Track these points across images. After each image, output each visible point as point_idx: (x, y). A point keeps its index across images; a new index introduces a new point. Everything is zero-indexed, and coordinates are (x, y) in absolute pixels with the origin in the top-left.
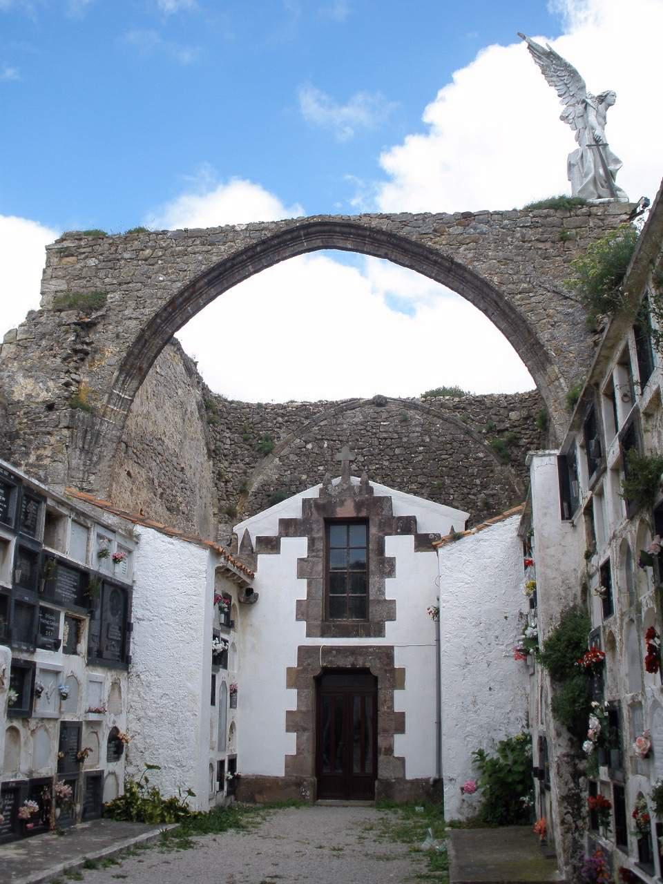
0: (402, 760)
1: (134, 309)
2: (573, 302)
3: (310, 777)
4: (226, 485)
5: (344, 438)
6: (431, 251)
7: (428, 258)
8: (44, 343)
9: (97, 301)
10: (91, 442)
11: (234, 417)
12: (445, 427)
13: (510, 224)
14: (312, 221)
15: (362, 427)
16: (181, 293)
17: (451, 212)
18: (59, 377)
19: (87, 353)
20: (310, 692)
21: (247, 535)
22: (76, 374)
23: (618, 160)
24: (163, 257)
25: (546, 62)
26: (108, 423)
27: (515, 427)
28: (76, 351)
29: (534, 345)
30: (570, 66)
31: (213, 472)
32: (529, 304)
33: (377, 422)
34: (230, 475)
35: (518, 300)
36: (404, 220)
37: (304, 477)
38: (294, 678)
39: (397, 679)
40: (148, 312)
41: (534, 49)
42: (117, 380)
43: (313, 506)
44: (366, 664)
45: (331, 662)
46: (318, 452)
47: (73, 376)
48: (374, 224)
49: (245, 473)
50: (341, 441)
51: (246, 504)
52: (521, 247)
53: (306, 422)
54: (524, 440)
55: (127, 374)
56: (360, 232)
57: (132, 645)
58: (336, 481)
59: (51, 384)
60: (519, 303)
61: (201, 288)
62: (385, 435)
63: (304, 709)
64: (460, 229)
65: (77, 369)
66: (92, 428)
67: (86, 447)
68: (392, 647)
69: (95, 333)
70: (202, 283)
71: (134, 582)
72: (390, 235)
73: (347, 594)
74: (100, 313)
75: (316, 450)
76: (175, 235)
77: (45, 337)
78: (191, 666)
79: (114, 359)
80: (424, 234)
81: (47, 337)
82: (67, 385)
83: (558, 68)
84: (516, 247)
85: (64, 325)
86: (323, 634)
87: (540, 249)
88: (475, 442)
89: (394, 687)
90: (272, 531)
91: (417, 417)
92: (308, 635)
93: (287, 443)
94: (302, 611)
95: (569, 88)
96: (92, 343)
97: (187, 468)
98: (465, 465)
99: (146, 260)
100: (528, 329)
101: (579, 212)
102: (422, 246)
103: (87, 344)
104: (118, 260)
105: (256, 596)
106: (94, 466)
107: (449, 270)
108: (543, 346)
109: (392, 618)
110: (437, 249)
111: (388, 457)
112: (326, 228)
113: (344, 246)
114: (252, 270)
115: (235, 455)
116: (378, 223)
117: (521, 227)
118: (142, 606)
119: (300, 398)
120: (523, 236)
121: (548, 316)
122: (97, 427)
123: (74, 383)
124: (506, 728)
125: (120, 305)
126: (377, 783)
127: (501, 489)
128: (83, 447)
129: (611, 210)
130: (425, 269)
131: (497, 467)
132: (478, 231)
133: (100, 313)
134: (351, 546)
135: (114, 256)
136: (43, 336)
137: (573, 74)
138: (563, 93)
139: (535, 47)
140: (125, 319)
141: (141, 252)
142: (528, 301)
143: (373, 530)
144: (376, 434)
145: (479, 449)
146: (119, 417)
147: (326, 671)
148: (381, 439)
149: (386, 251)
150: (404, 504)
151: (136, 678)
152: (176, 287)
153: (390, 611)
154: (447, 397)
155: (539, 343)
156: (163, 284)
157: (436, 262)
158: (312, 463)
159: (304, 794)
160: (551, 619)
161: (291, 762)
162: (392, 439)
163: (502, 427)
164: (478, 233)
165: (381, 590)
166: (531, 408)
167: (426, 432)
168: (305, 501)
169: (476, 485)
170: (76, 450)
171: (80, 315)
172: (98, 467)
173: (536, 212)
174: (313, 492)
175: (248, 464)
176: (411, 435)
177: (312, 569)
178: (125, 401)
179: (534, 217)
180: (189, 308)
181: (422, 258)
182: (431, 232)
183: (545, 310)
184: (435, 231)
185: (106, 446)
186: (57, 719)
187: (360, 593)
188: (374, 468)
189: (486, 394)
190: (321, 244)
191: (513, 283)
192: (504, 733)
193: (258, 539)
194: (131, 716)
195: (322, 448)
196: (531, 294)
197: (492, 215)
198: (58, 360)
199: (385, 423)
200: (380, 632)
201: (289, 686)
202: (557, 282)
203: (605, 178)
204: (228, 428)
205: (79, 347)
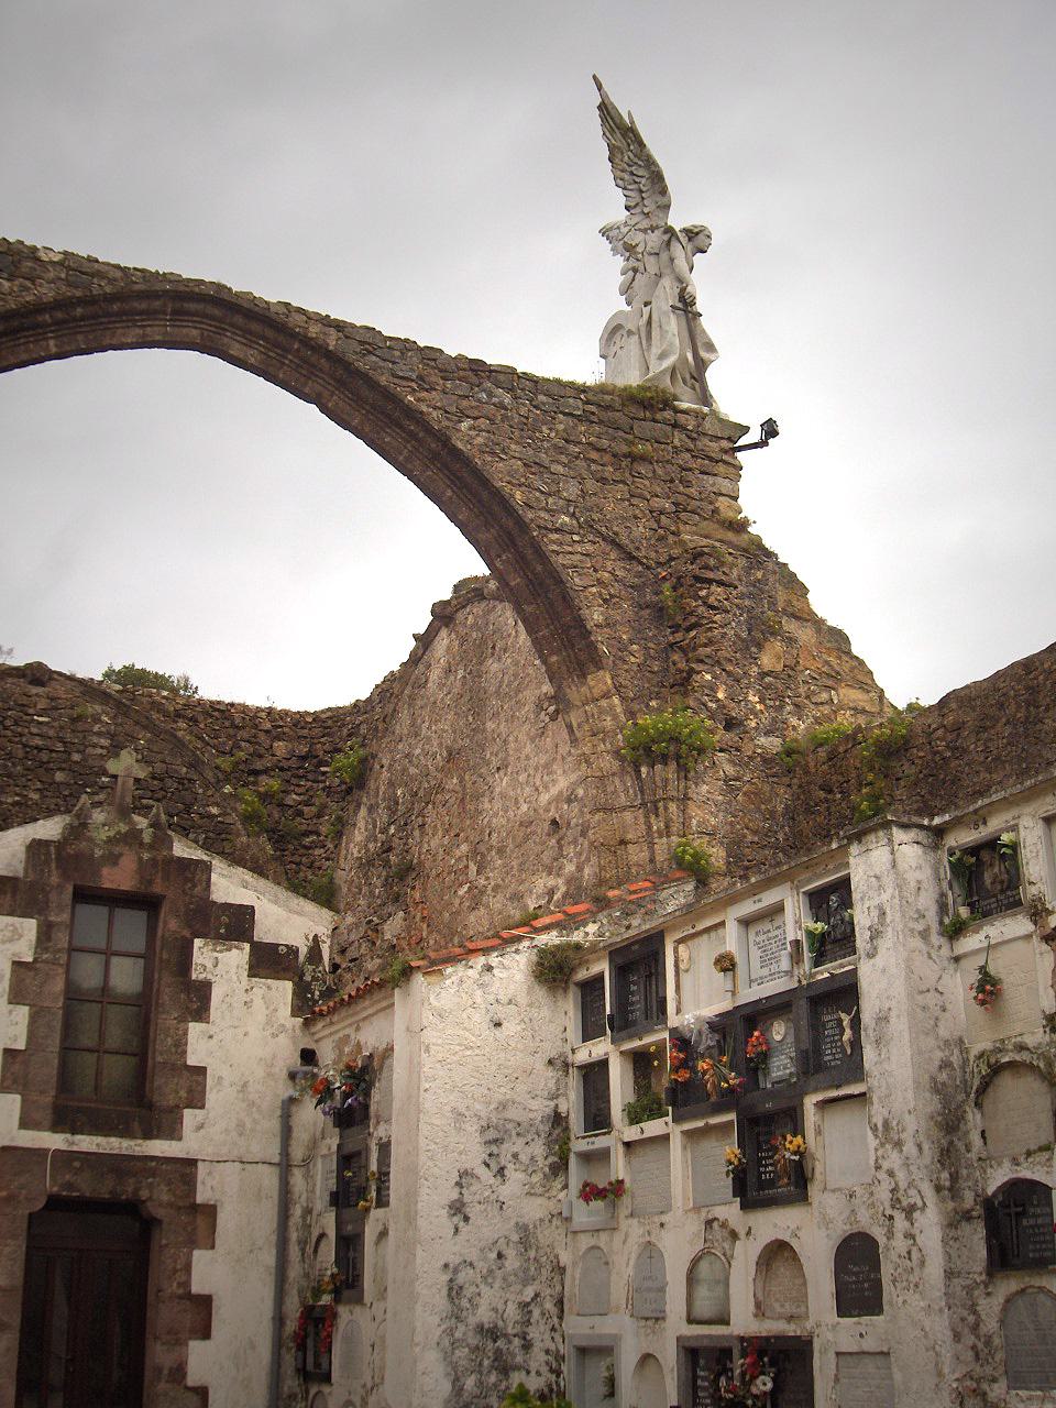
2: (640, 568)
13: (548, 403)
14: (197, 290)
17: (451, 351)
23: (713, 345)
25: (619, 142)
30: (654, 163)
32: (571, 553)
33: (27, 714)
41: (609, 113)
44: (141, 1193)
48: (314, 330)
54: (294, 796)
56: (281, 338)
62: (38, 741)
83: (636, 160)
84: (555, 446)
88: (206, 786)
89: (192, 1243)
92: (25, 1124)
95: (643, 198)
101: (658, 416)
102: (396, 400)
110: (422, 412)
111: (39, 785)
114: (54, 350)
121: (600, 582)
132: (495, 400)
137: (657, 178)
138: (633, 204)
139: (612, 112)
142: (570, 549)
143: (171, 924)
144: (21, 735)
145: (212, 799)
147: (54, 1203)
148: (30, 747)
157: (413, 435)
162: (52, 751)
163: (258, 765)
165: (181, 1045)
166: (316, 741)
174: (49, 829)
176: (90, 750)
183: (596, 571)
184: (421, 378)
188: (10, 800)
191: (548, 511)
196: (576, 538)
199: (41, 719)
200: (174, 1132)
203: (693, 370)
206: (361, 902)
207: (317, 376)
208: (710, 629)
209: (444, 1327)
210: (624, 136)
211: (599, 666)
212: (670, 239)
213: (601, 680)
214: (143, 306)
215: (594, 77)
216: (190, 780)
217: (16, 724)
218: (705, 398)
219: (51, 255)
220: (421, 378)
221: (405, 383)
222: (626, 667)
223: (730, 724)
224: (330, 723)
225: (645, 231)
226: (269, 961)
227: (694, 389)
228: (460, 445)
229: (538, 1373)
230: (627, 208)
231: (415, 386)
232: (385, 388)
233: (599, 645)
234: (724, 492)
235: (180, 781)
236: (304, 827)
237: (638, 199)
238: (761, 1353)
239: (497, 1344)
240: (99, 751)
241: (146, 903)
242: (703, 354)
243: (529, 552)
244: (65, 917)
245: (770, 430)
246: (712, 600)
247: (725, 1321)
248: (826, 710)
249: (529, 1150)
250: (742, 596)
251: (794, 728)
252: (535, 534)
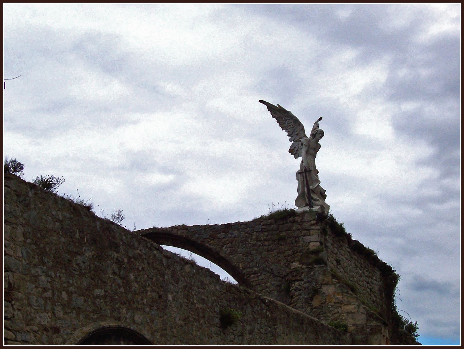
121: (267, 287)
184: (210, 236)
196: (259, 274)
197: (241, 225)
215: (260, 101)
221: (206, 240)
228: (223, 255)
231: (208, 240)
248: (336, 316)
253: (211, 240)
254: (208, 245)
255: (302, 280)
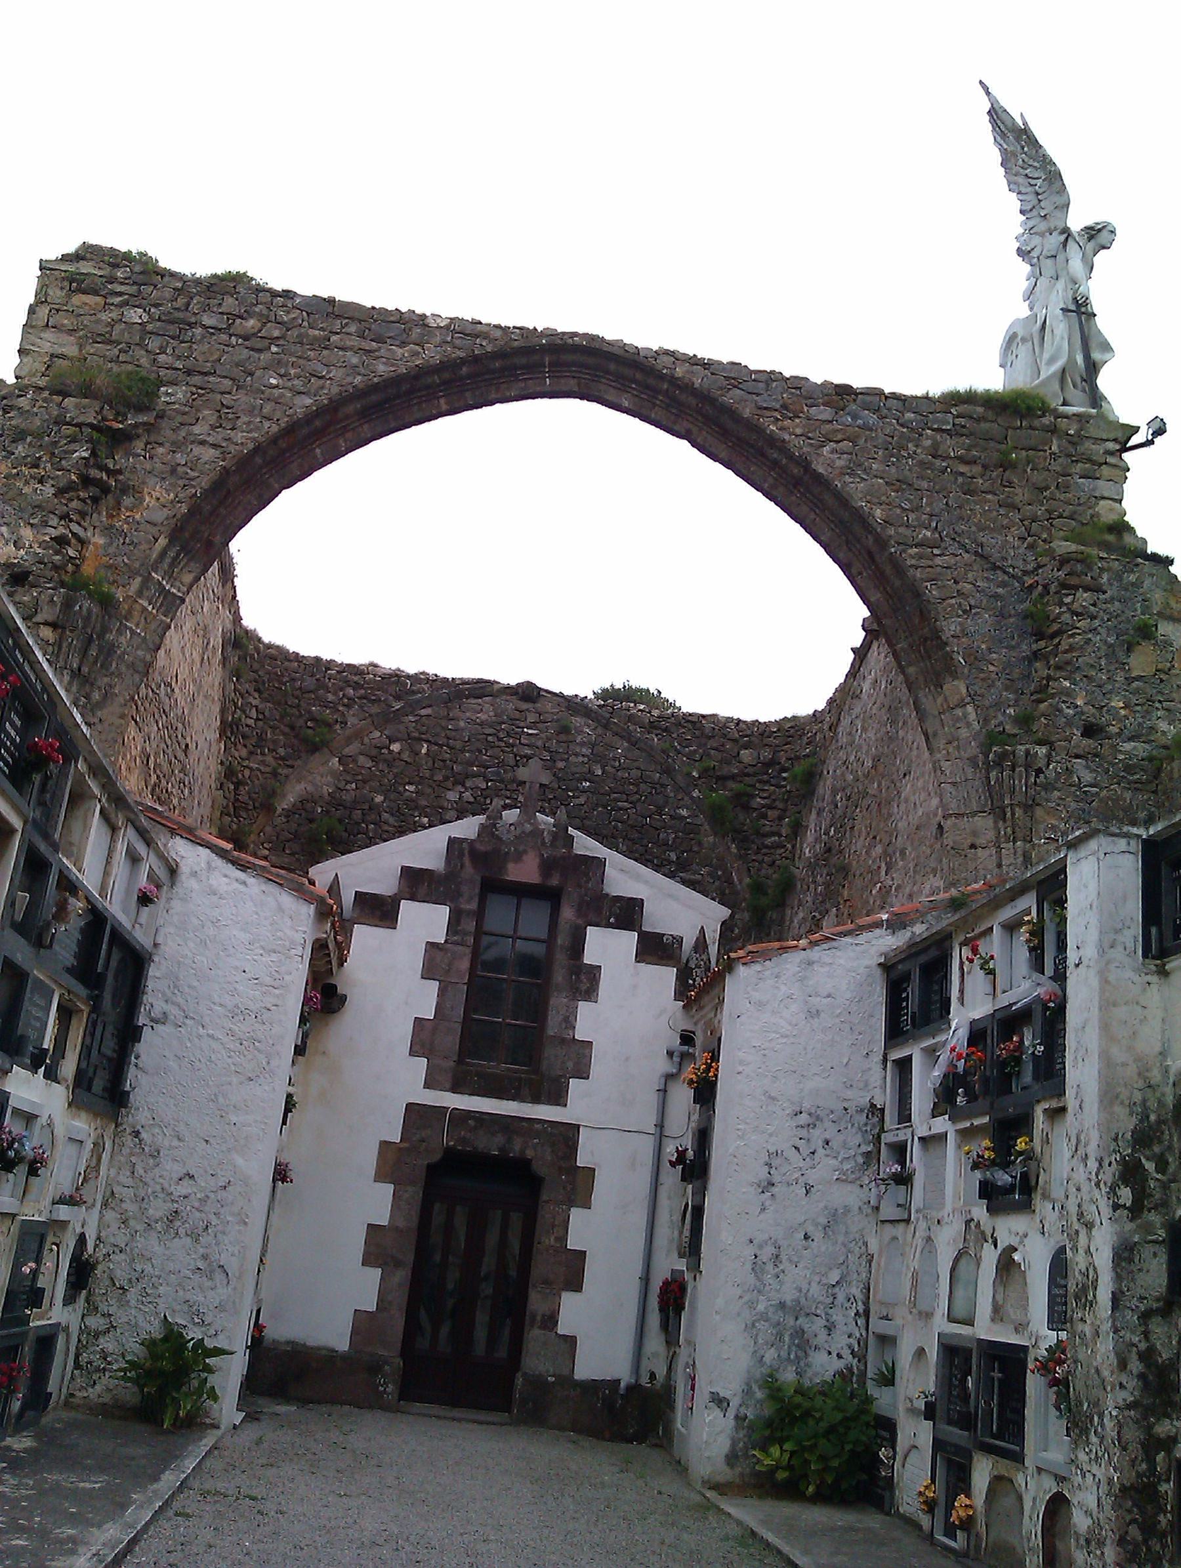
0: (571, 1341)
1: (213, 427)
3: (390, 1352)
4: (236, 789)
5: (458, 745)
6: (772, 441)
7: (763, 455)
8: (20, 450)
9: (139, 396)
10: (95, 662)
11: (269, 673)
12: (629, 755)
15: (491, 731)
16: (310, 418)
17: (817, 379)
18: (46, 522)
19: (106, 490)
20: (414, 1193)
21: (334, 888)
22: (79, 524)
24: (281, 342)
25: (1014, 147)
26: (133, 632)
27: (748, 775)
28: (86, 481)
29: (926, 639)
31: (222, 763)
34: (247, 773)
35: (912, 557)
36: (732, 375)
37: (379, 799)
38: (391, 1163)
39: (579, 1186)
40: (243, 438)
42: (163, 554)
43: (466, 852)
45: (463, 1141)
46: (409, 760)
47: (75, 528)
48: (679, 371)
49: (275, 774)
50: (451, 748)
51: (268, 829)
52: (930, 466)
53: (397, 705)
55: (183, 548)
57: (132, 1069)
58: (511, 815)
59: (27, 533)
60: (913, 562)
61: (347, 417)
63: (401, 1223)
64: (826, 413)
65: (83, 514)
66: (101, 636)
67: (85, 670)
68: (578, 1126)
69: (128, 454)
70: (350, 409)
71: (156, 945)
72: (704, 397)
73: (505, 1018)
74: (143, 418)
75: (406, 756)
76: (308, 305)
77: (24, 439)
78: (250, 1125)
79: (160, 513)
80: (766, 408)
81: (29, 439)
82: (61, 541)
84: (922, 463)
85: (68, 424)
86: (456, 1087)
87: (962, 474)
88: (678, 788)
89: (571, 1203)
90: (385, 885)
91: (586, 730)
92: (427, 1085)
93: (358, 735)
94: (423, 1039)
95: (1040, 201)
96: (120, 472)
97: (192, 746)
98: (658, 824)
99: (246, 338)
100: (921, 611)
101: (1036, 423)
102: (759, 430)
103: (110, 472)
104: (190, 324)
105: (344, 998)
106: (92, 710)
107: (797, 482)
108: (946, 644)
109: (583, 1073)
112: (591, 361)
113: (615, 400)
114: (444, 407)
115: (260, 738)
116: (687, 372)
117: (933, 430)
118: (164, 994)
119: (389, 661)
120: (936, 445)
121: (960, 593)
122: (110, 637)
123: (73, 541)
124: (827, 1314)
125: (184, 414)
126: (519, 1381)
127: (709, 874)
128: (79, 670)
129: (1092, 431)
130: (753, 473)
131: (707, 836)
132: (860, 422)
133: (143, 418)
134: (521, 933)
135: (180, 315)
136: (19, 436)
137: (1054, 177)
139: (1003, 116)
140: (192, 442)
141: (238, 321)
142: (930, 563)
143: (568, 913)
145: (681, 803)
146: (153, 626)
149: (690, 426)
150: (625, 877)
151: (130, 1137)
152: (300, 404)
153: (579, 1058)
154: (642, 707)
155: (940, 638)
156: (276, 392)
157: (775, 464)
158: (395, 776)
159: (381, 1389)
160: (1116, 1139)
161: (363, 1324)
163: (725, 770)
164: (858, 427)
165: (569, 1022)
167: (597, 758)
168: (452, 842)
169: (670, 862)
170: (65, 672)
171: (105, 412)
172: (99, 713)
173: (963, 408)
174: (467, 828)
175: (282, 758)
177: (450, 965)
178: (170, 598)
179: (958, 417)
180: (318, 451)
181: (752, 450)
182: (778, 406)
183: (956, 582)
184: (785, 406)
185: (120, 675)
186: (14, 1216)
187: (527, 1020)
189: (704, 713)
190: (576, 389)
192: (824, 1322)
193: (359, 895)
194: (110, 1215)
195: (417, 753)
196: (936, 551)
197: (886, 397)
198: (49, 491)
199: (530, 731)
201: (380, 1177)
202: (983, 538)
204: (257, 690)
205: (94, 473)
206: (809, 899)
207: (686, 414)
208: (1073, 635)
209: (746, 1299)
210: (1018, 139)
211: (955, 675)
212: (1067, 239)
213: (957, 688)
214: (524, 361)
215: (981, 82)
216: (662, 785)
217: (508, 735)
218: (1096, 399)
219: (439, 320)
220: (785, 406)
221: (768, 413)
222: (982, 675)
223: (1090, 731)
224: (791, 729)
225: (1042, 235)
226: (655, 948)
227: (1084, 391)
229: (839, 1356)
230: (1022, 212)
232: (748, 420)
233: (955, 656)
234: (1106, 495)
235: (654, 785)
236: (767, 829)
237: (1035, 202)
238: (995, 1358)
239: (798, 1322)
240: (581, 759)
241: (550, 896)
242: (1096, 355)
243: (888, 570)
244: (474, 906)
245: (1160, 431)
246: (1075, 606)
247: (970, 1322)
249: (841, 1137)
250: (1112, 600)
251: (1164, 733)
252: (893, 550)
253: (785, 417)
254: (772, 427)
255: (1099, 590)
